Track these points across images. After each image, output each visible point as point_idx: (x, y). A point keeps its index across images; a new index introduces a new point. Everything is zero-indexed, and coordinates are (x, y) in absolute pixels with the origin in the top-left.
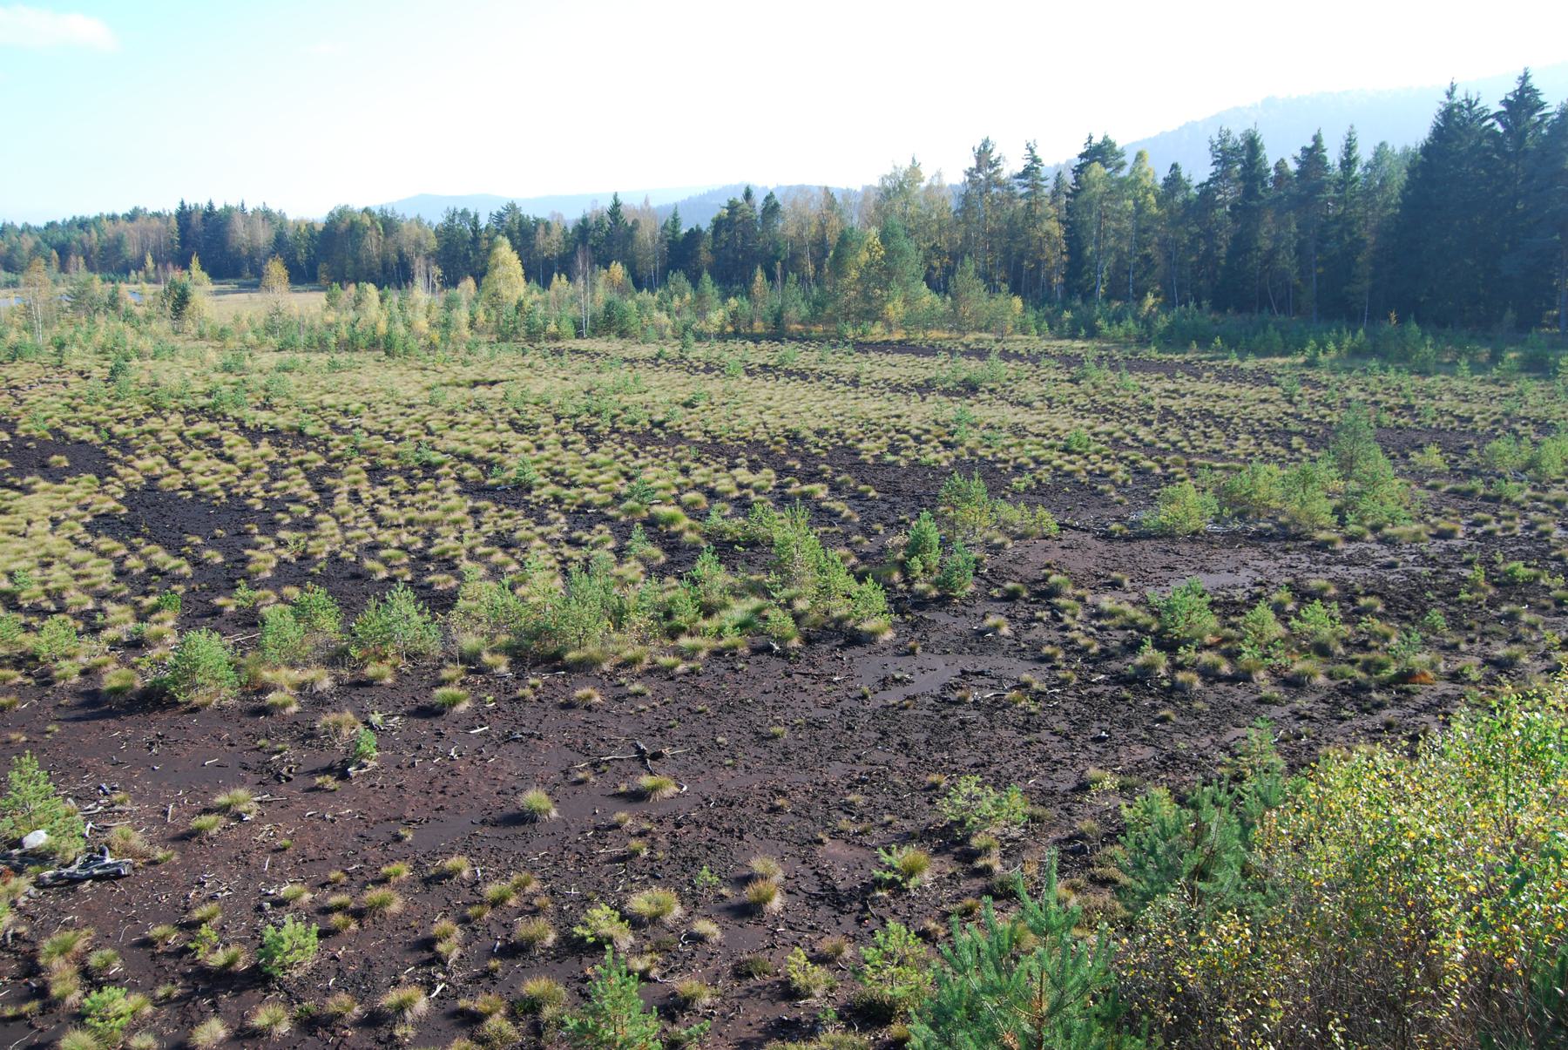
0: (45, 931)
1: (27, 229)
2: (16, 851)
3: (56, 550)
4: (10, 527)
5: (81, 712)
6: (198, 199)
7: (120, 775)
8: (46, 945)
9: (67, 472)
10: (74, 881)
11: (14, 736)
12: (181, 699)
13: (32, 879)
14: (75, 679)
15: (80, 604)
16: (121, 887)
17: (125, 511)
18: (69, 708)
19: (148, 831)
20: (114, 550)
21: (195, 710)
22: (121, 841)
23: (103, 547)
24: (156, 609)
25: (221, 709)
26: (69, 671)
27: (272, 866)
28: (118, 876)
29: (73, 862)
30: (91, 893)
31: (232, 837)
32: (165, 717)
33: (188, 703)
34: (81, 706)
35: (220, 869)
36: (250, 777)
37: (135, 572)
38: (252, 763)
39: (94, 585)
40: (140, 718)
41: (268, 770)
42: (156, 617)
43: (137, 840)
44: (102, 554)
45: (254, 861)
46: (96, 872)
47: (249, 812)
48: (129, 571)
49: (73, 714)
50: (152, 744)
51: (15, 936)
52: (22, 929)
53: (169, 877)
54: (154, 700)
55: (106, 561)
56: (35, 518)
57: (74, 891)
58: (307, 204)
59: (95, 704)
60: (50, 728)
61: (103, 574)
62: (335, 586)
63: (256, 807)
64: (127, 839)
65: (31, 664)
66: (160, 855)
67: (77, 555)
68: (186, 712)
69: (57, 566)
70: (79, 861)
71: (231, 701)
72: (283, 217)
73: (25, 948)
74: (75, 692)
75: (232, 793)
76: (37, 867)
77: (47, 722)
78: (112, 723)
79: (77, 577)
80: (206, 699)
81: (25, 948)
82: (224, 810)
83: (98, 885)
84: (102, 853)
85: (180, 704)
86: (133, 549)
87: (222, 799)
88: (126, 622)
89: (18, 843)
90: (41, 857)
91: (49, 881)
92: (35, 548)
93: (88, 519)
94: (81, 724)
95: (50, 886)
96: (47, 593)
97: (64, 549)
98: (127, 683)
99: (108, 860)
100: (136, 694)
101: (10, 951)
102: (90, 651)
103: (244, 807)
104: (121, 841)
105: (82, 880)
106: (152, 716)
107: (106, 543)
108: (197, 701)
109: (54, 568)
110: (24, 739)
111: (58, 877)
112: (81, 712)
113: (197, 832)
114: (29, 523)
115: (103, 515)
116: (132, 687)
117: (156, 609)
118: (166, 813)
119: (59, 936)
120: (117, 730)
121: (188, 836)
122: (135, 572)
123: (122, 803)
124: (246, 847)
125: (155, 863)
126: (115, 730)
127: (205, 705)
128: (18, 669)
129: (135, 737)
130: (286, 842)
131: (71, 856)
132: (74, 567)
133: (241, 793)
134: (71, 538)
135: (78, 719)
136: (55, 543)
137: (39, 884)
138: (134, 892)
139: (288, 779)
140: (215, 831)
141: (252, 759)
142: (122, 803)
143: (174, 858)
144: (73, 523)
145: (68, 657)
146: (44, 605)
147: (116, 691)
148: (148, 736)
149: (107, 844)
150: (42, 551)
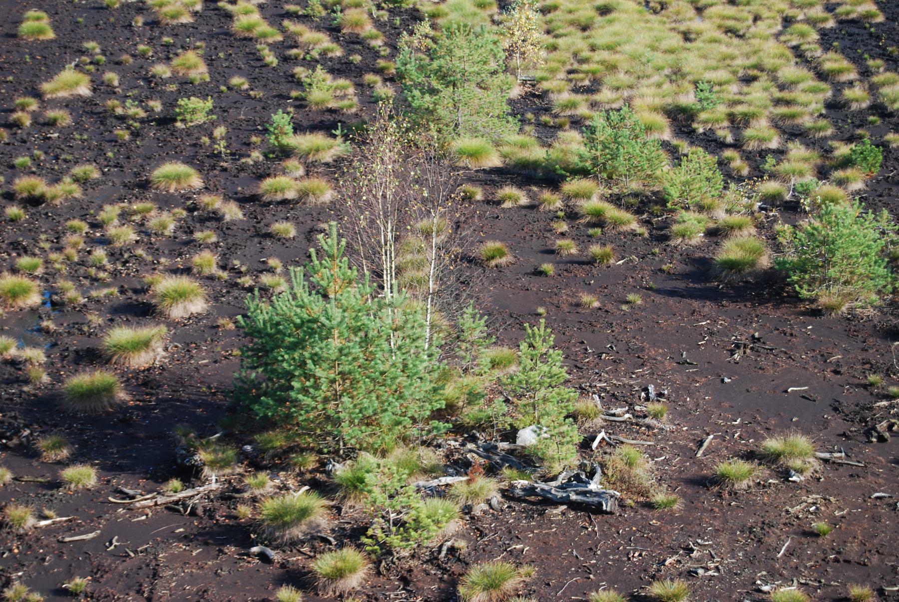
0: (483, 553)
2: (504, 445)
3: (769, 62)
4: (730, 23)
5: (681, 285)
7: (678, 378)
8: (474, 573)
10: (548, 501)
11: (586, 298)
12: (805, 293)
13: (504, 485)
14: (698, 239)
15: (761, 140)
16: (596, 525)
17: (880, 19)
18: (670, 275)
19: (667, 462)
20: (840, 72)
21: (816, 313)
22: (620, 465)
23: (828, 66)
24: (846, 163)
25: (851, 318)
26: (691, 227)
27: (790, 553)
28: (597, 509)
29: (554, 478)
30: (559, 524)
31: (762, 498)
32: (774, 314)
33: (812, 301)
34: (685, 276)
35: (723, 539)
36: (837, 423)
37: (854, 106)
38: (848, 405)
39: (793, 116)
40: (743, 308)
41: (863, 420)
42: (839, 174)
43: (643, 470)
44: (822, 76)
45: (770, 540)
46: (573, 497)
47: (800, 471)
48: (846, 104)
49: (671, 285)
50: (738, 346)
51: (452, 550)
52: (461, 544)
53: (657, 530)
54: (769, 288)
55: (823, 85)
56: (765, 13)
57: (541, 514)
59: (707, 279)
60: (631, 297)
61: (810, 101)
62: (259, 64)
63: (817, 465)
64: (630, 464)
65: (657, 208)
66: (659, 497)
67: (790, 71)
68: (803, 314)
69: (764, 81)
70: (562, 479)
71: (870, 312)
73: (455, 568)
74: (689, 258)
75: (791, 439)
76: (515, 472)
77: (634, 289)
78: (708, 307)
79: (778, 102)
80: (834, 300)
81: (455, 568)
82: (770, 459)
83: (571, 515)
84: (591, 475)
85: (802, 300)
86: (866, 73)
87: (773, 444)
88: (801, 174)
89: (511, 435)
90: (525, 460)
91: (519, 492)
92: (747, 56)
93: (831, 24)
94: (671, 301)
95: (519, 500)
96: (731, 117)
97: (778, 62)
98: (749, 257)
99: (594, 486)
100: (755, 275)
101: (439, 567)
102: (733, 205)
103: (798, 463)
104: (620, 465)
105: (555, 503)
106: (761, 310)
107: (833, 61)
108: (824, 300)
109: (756, 84)
110: (596, 304)
111: (531, 490)
112: (681, 285)
113: (719, 480)
114: (757, 18)
115: (853, 21)
116: (753, 264)
117: (846, 163)
118: (700, 443)
119: (497, 566)
120: (709, 317)
121: (709, 482)
122: (854, 106)
123: (656, 416)
124: (771, 517)
125: (650, 506)
126: (705, 317)
127: (831, 308)
128: (639, 212)
129: (725, 332)
130: (820, 525)
131: (555, 472)
132: (782, 87)
133: (802, 442)
134: (796, 48)
135: (672, 293)
136: (771, 51)
137: (507, 494)
138: (605, 536)
139: (881, 439)
140: (744, 484)
141: (850, 398)
142: (656, 416)
143: (676, 507)
144: (805, 27)
145: (701, 208)
146: (720, 133)
147: (732, 266)
148: (741, 334)
149: (603, 466)
150: (753, 60)
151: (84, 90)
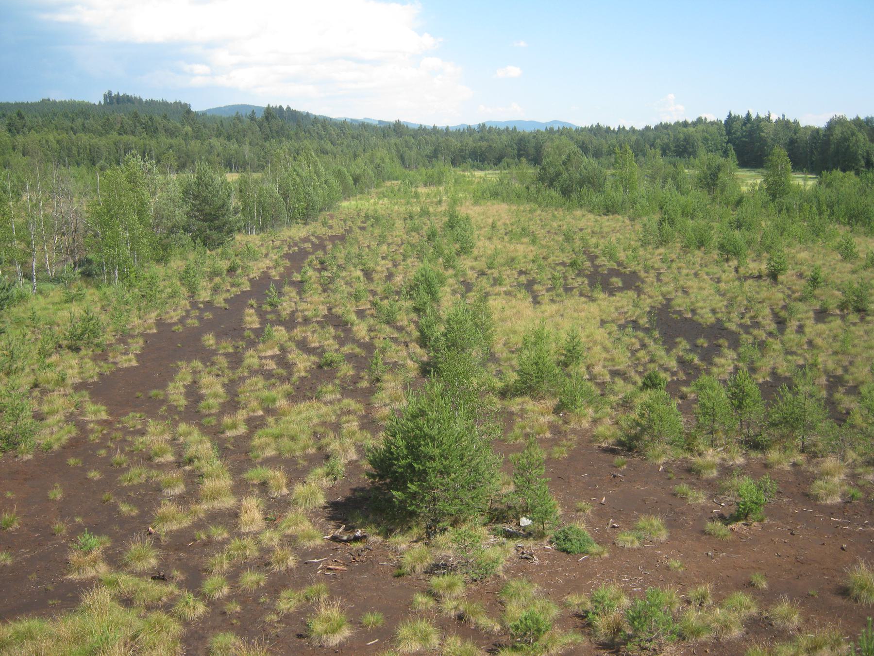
1: (633, 130)
6: (481, 122)
9: (620, 289)
58: (813, 117)
72: (796, 123)
151: (231, 350)
